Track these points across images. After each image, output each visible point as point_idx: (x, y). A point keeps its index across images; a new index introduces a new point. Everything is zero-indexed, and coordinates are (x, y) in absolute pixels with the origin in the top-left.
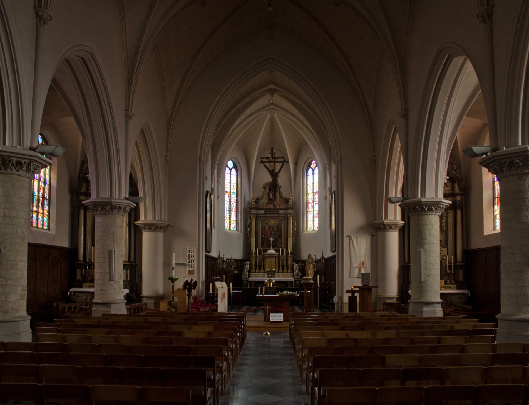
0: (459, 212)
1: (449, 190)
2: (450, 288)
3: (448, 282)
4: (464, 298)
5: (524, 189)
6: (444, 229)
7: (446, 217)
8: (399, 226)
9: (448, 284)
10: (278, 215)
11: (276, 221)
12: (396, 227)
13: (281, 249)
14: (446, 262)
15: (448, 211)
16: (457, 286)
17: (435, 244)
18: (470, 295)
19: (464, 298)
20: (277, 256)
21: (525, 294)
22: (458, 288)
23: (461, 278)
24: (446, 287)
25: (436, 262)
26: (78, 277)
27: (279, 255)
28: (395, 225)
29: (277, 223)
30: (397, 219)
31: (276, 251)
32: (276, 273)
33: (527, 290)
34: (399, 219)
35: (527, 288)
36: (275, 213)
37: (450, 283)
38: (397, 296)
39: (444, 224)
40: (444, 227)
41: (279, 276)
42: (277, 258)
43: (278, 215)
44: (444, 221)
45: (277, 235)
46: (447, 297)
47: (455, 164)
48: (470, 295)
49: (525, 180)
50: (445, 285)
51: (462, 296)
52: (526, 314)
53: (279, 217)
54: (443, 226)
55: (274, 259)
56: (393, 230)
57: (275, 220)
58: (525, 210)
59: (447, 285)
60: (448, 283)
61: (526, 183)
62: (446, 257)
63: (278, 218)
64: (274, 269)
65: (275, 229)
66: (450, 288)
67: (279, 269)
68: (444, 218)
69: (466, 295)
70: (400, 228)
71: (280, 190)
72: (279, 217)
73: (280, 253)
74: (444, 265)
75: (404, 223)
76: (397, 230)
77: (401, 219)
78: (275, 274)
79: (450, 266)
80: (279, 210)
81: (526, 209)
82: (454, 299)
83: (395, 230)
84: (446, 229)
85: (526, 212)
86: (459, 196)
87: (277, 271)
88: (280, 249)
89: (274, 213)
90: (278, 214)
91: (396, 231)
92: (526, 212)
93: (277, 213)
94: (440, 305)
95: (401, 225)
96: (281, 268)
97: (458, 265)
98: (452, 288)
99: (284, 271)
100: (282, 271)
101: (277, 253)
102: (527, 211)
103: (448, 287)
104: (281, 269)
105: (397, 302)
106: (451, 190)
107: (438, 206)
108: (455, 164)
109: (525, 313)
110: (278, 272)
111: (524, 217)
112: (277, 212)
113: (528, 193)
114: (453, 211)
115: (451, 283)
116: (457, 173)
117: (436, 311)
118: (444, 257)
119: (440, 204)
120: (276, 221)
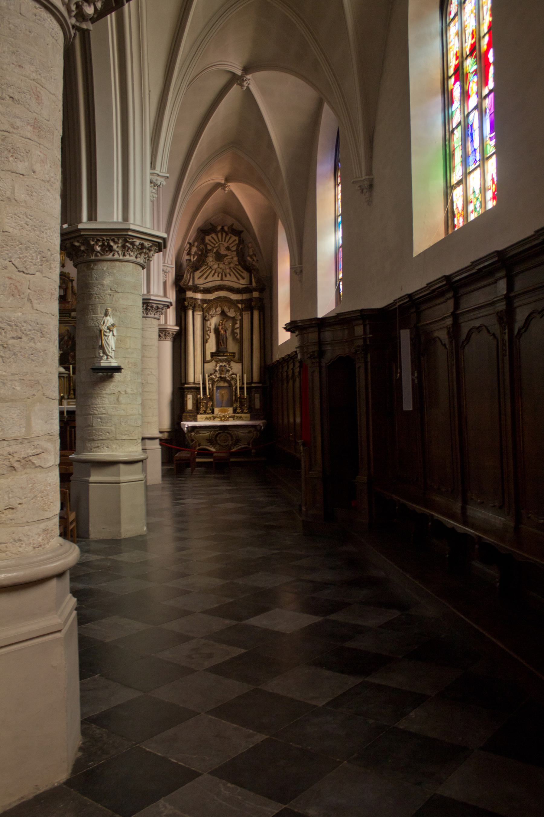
0: (256, 314)
1: (246, 283)
2: (240, 418)
3: (239, 411)
4: (255, 432)
5: (91, 282)
6: (238, 337)
7: (241, 321)
8: (171, 333)
9: (238, 413)
10: (70, 319)
11: (68, 328)
12: (167, 334)
13: (71, 366)
14: (236, 383)
15: (244, 313)
16: (251, 416)
17: (147, 357)
18: (263, 428)
19: (255, 432)
20: (66, 376)
21: (89, 426)
22: (252, 419)
23: (257, 404)
24: (235, 418)
25: (147, 383)
26: (190, 405)
27: (69, 374)
28: (163, 331)
29: (68, 330)
30: (168, 323)
31: (65, 368)
32: (65, 399)
33: (92, 420)
34: (171, 324)
35: (91, 416)
36: (65, 316)
37: (211, 412)
38: (168, 430)
39: (238, 331)
40: (237, 335)
41: (68, 404)
42: (65, 378)
43: (70, 319)
44: (237, 326)
45: (69, 347)
46: (231, 430)
47: (251, 247)
48: (263, 428)
49: (93, 269)
50: (234, 415)
51: (252, 429)
52: (90, 452)
53: (70, 322)
54: (237, 333)
55: (62, 381)
56: (162, 339)
57: (66, 326)
58: (91, 311)
59: (236, 415)
60: (238, 411)
61: (93, 274)
62: (236, 375)
63: (70, 323)
64: (62, 393)
65: (66, 338)
66: (241, 418)
67: (69, 394)
68: (238, 322)
69: (258, 427)
70: (174, 336)
71: (72, 284)
72: (70, 322)
73: (70, 372)
74: (234, 388)
75: (178, 328)
76: (169, 338)
77: (175, 323)
78: (63, 400)
79: (242, 389)
80: (71, 311)
81: (92, 310)
82: (241, 433)
83: (165, 339)
84: (240, 336)
85: (92, 313)
86: (256, 292)
87: (66, 397)
88: (70, 366)
89: (64, 316)
90: (70, 317)
91: (167, 339)
92: (92, 313)
93: (67, 316)
94: (157, 441)
95: (175, 331)
96: (72, 392)
97: (253, 386)
98: (244, 418)
99: (70, 397)
100: (73, 397)
101: (67, 372)
102: (93, 311)
103: (237, 417)
104: (72, 394)
105: (169, 438)
106: (249, 283)
107: (148, 306)
108: (251, 247)
109: (90, 452)
110: (68, 398)
111: (90, 320)
112: (68, 315)
113: (95, 287)
114: (249, 313)
115: (242, 412)
116: (254, 260)
117: (146, 450)
118: (234, 376)
119: (149, 302)
120: (68, 328)
